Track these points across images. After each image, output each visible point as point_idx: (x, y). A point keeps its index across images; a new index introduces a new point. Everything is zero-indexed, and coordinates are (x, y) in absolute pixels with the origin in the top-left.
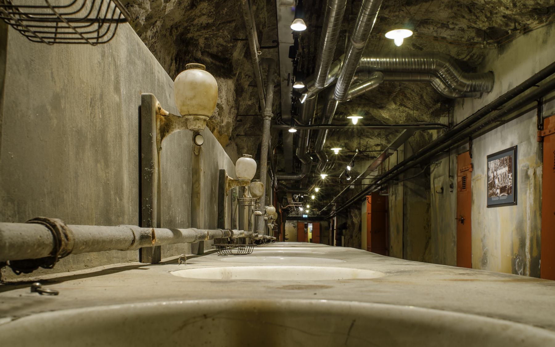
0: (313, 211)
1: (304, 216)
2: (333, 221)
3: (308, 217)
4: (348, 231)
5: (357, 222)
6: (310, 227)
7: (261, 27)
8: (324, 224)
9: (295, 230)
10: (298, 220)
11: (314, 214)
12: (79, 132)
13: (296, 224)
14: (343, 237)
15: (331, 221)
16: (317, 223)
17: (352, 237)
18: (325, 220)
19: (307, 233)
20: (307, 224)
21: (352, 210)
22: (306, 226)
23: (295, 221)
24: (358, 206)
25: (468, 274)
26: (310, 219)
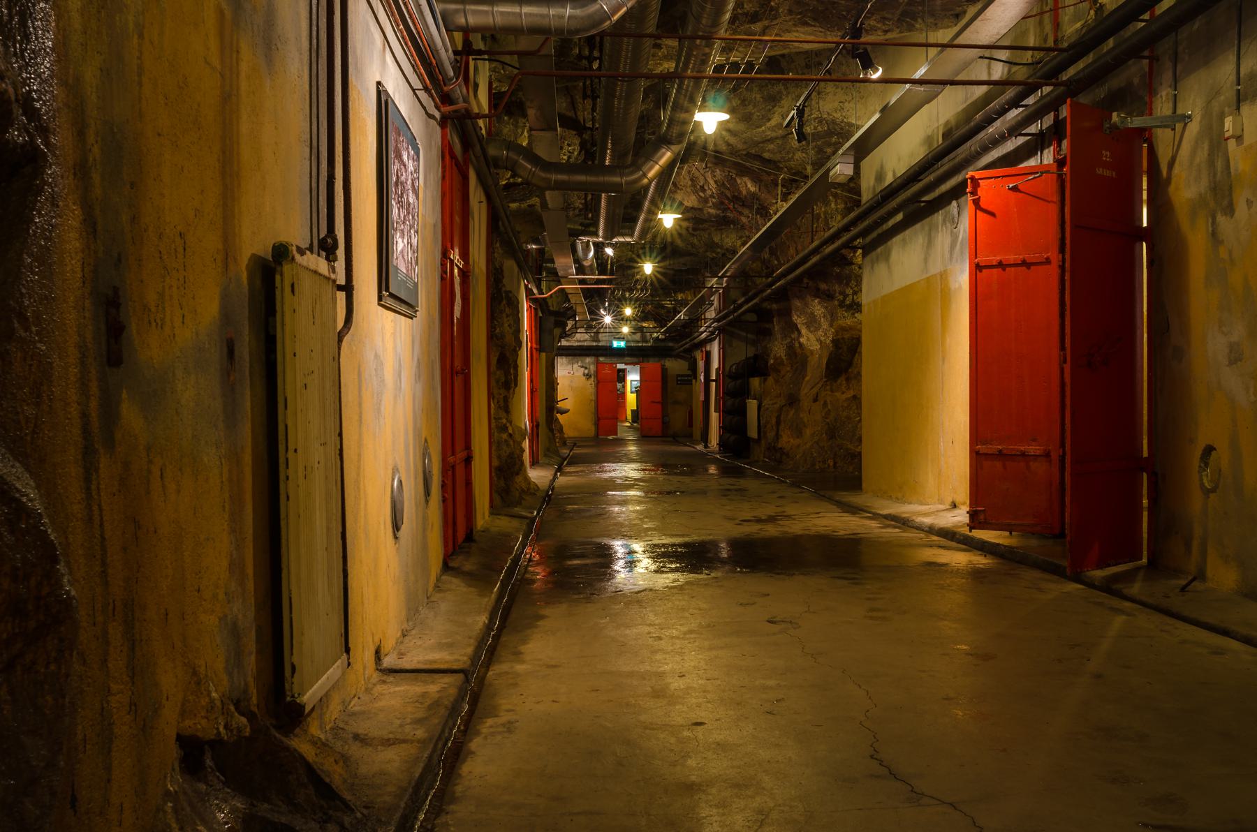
0: (641, 329)
1: (616, 344)
2: (708, 355)
3: (628, 348)
4: (770, 380)
5: (816, 346)
6: (633, 377)
7: (589, 145)
8: (675, 366)
9: (590, 386)
10: (597, 356)
11: (644, 339)
12: (312, 252)
13: (592, 368)
14: (752, 404)
15: (699, 355)
16: (653, 364)
17: (793, 400)
18: (678, 356)
19: (623, 395)
20: (624, 371)
21: (797, 303)
22: (621, 376)
23: (588, 360)
24: (823, 286)
25: (398, 388)
26: (634, 354)
